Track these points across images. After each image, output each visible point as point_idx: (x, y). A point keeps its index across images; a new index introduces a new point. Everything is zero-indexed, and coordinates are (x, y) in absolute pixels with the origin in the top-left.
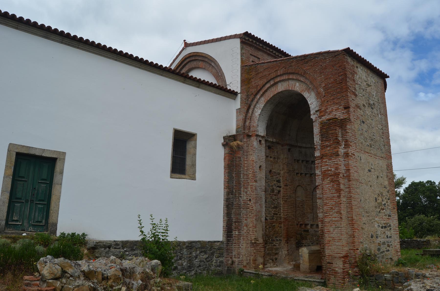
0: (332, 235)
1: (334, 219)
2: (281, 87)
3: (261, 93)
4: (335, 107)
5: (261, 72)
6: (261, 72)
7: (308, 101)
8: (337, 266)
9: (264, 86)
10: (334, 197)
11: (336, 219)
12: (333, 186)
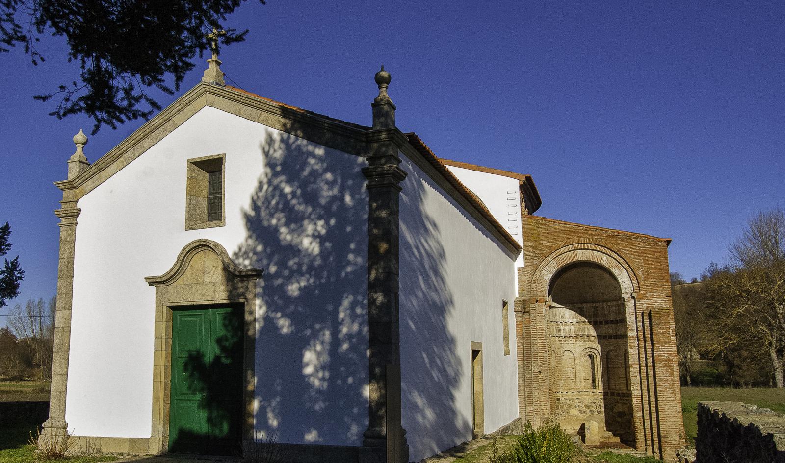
0: (667, 413)
1: (668, 399)
2: (582, 255)
4: (655, 294)
7: (619, 279)
8: (672, 439)
10: (668, 380)
11: (670, 399)
12: (667, 370)
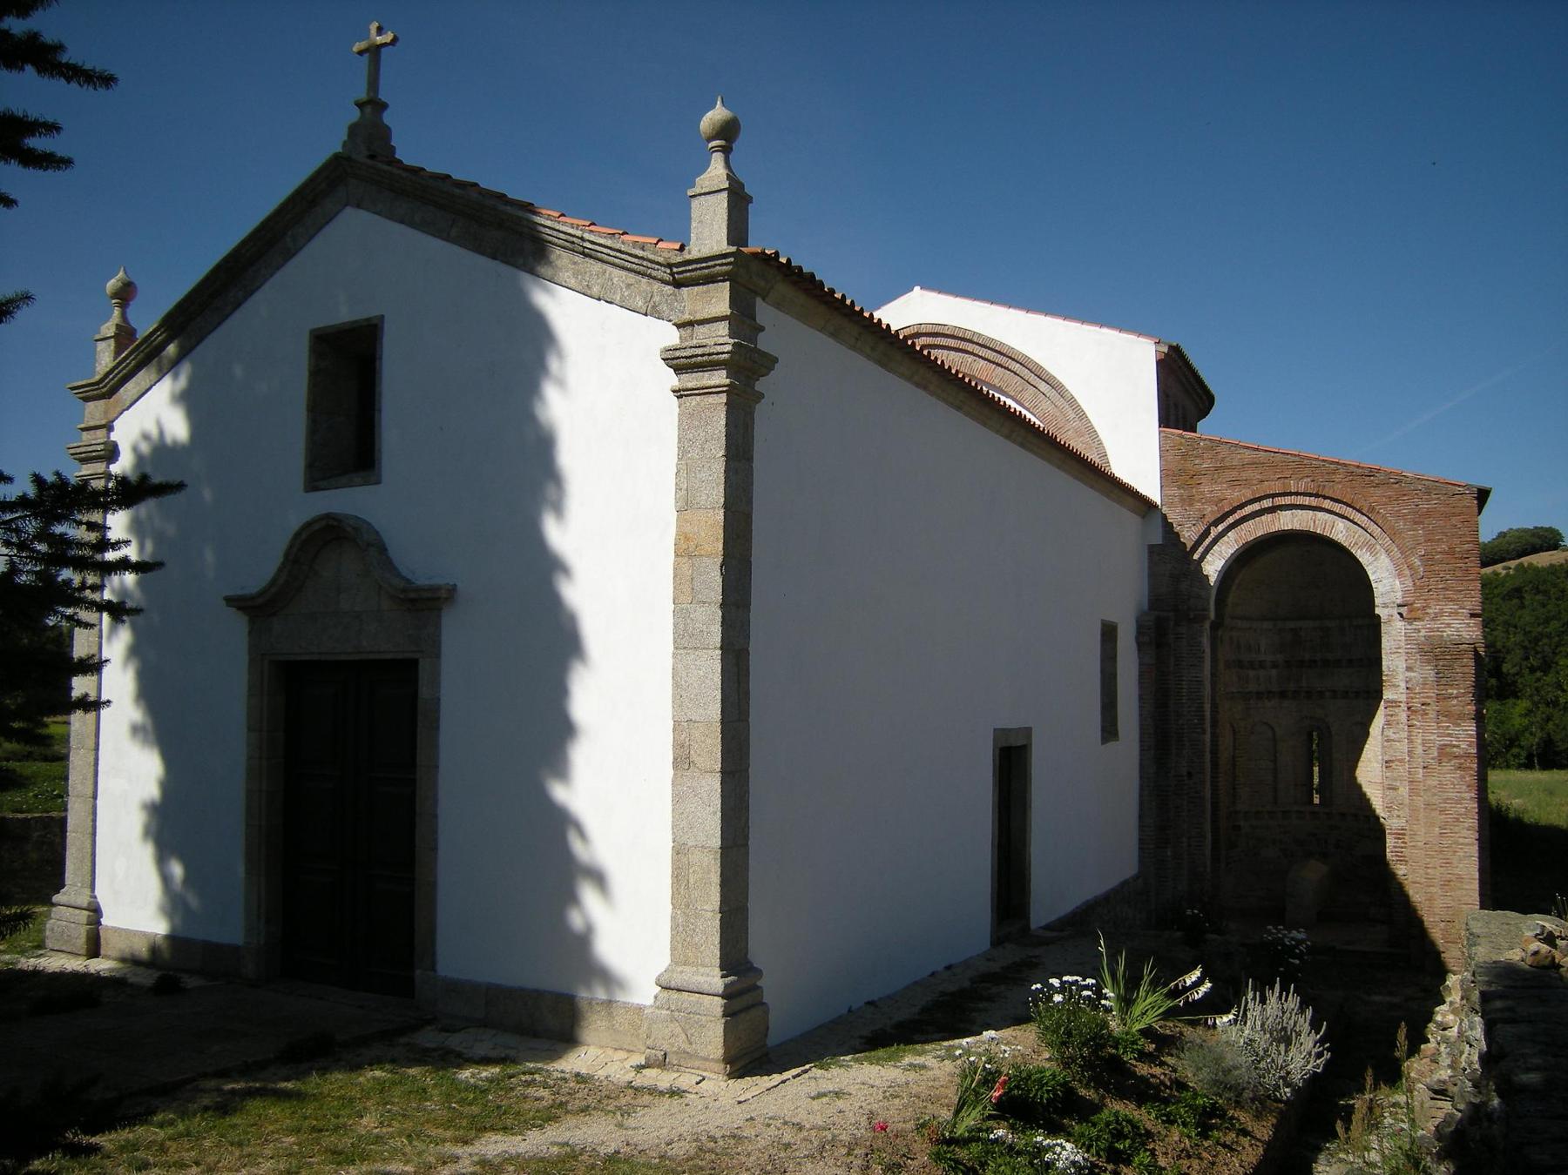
3: (1231, 520)
5: (1232, 468)
6: (1232, 468)
9: (1242, 506)
12: (1462, 777)
